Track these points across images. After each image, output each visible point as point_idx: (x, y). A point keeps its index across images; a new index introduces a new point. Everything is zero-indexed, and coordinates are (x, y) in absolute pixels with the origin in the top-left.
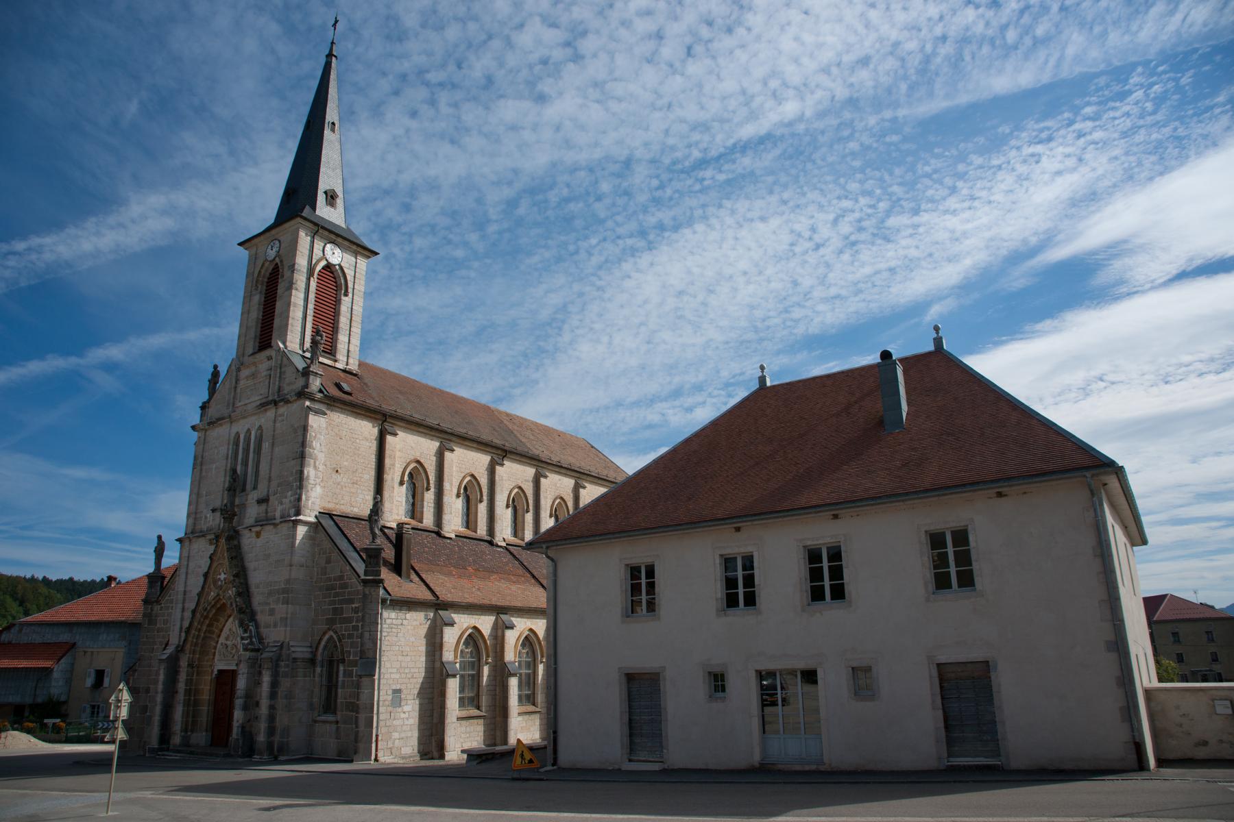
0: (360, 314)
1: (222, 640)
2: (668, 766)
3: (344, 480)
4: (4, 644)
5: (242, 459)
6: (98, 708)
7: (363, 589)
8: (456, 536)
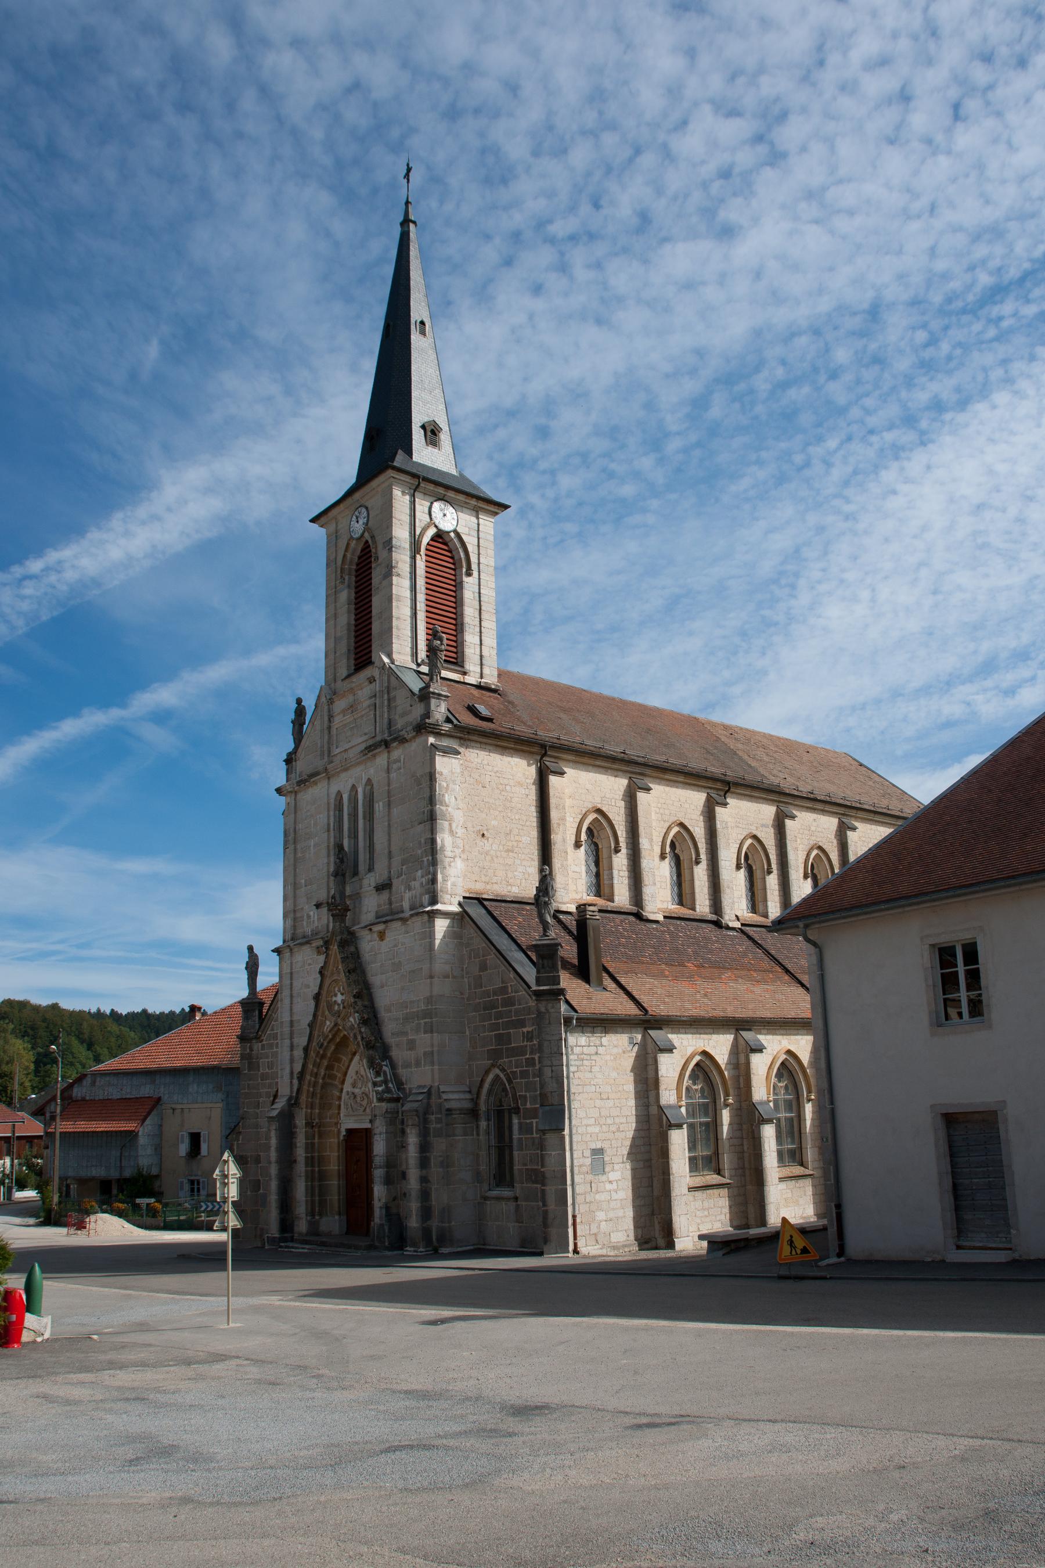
0: (493, 600)
1: (347, 1087)
2: (1020, 1256)
3: (495, 847)
4: (77, 1101)
5: (349, 829)
6: (198, 1184)
7: (537, 1004)
8: (665, 917)
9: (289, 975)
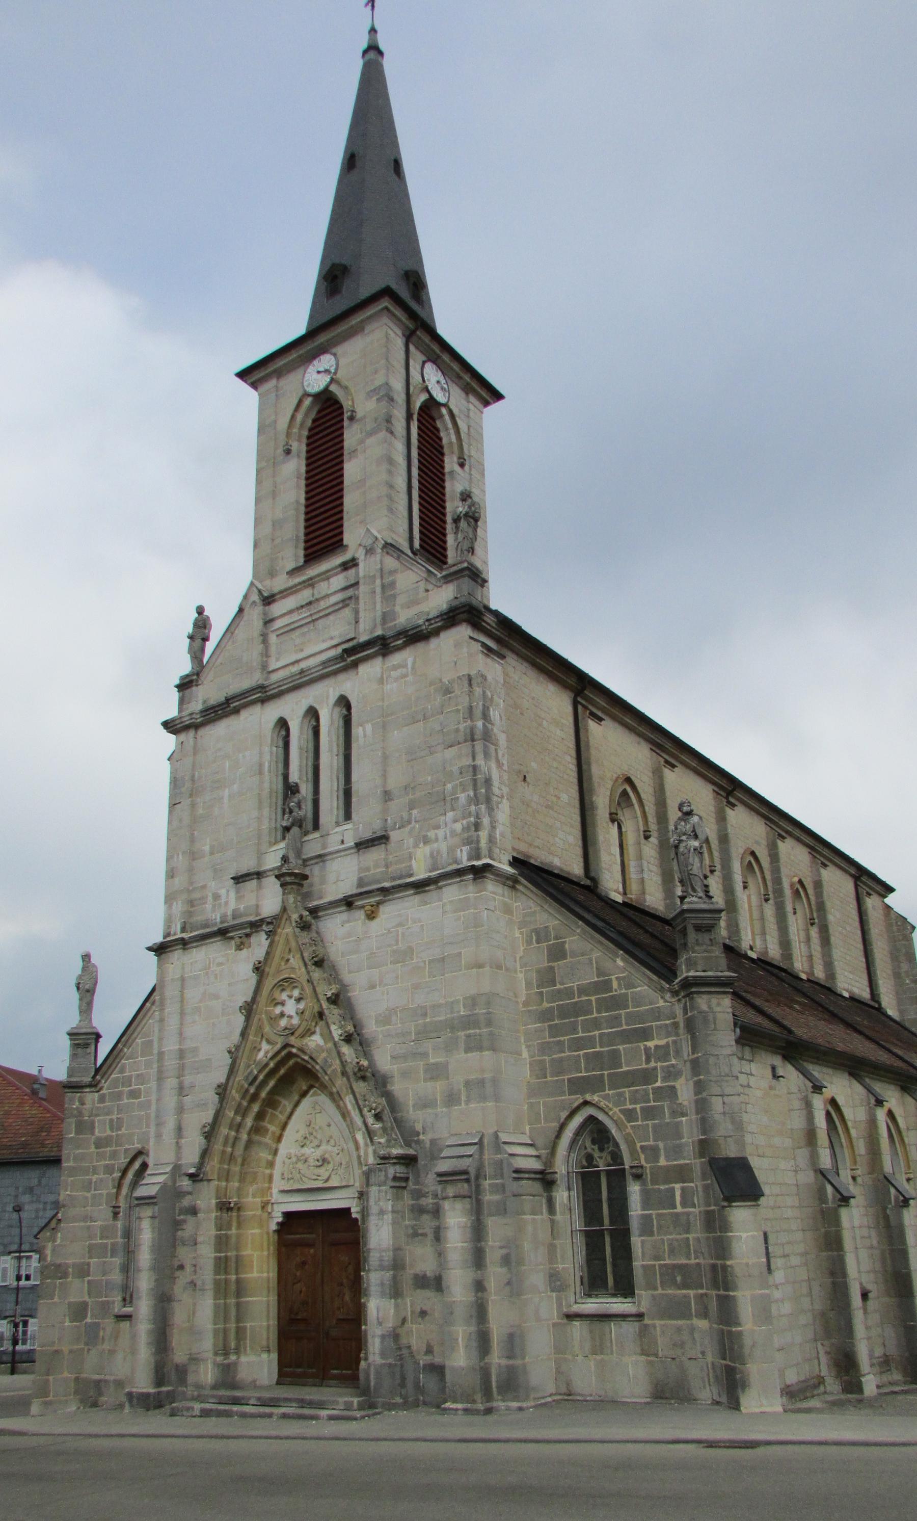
9: (179, 983)
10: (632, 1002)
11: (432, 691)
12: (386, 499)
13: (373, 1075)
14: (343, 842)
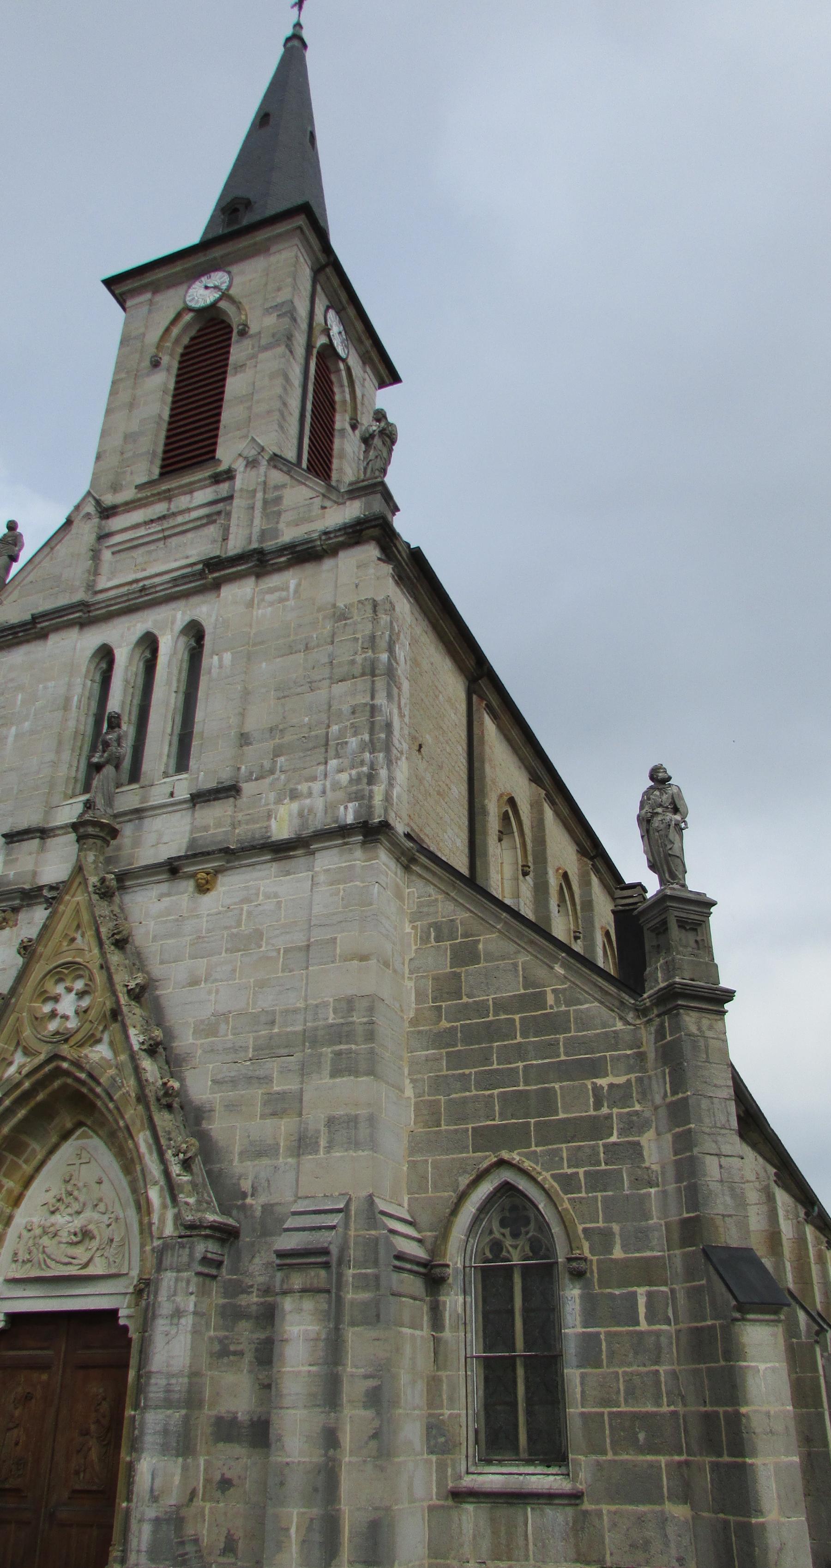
10: (576, 1023)
11: (321, 618)
12: (277, 413)
13: (182, 1108)
14: (172, 795)
